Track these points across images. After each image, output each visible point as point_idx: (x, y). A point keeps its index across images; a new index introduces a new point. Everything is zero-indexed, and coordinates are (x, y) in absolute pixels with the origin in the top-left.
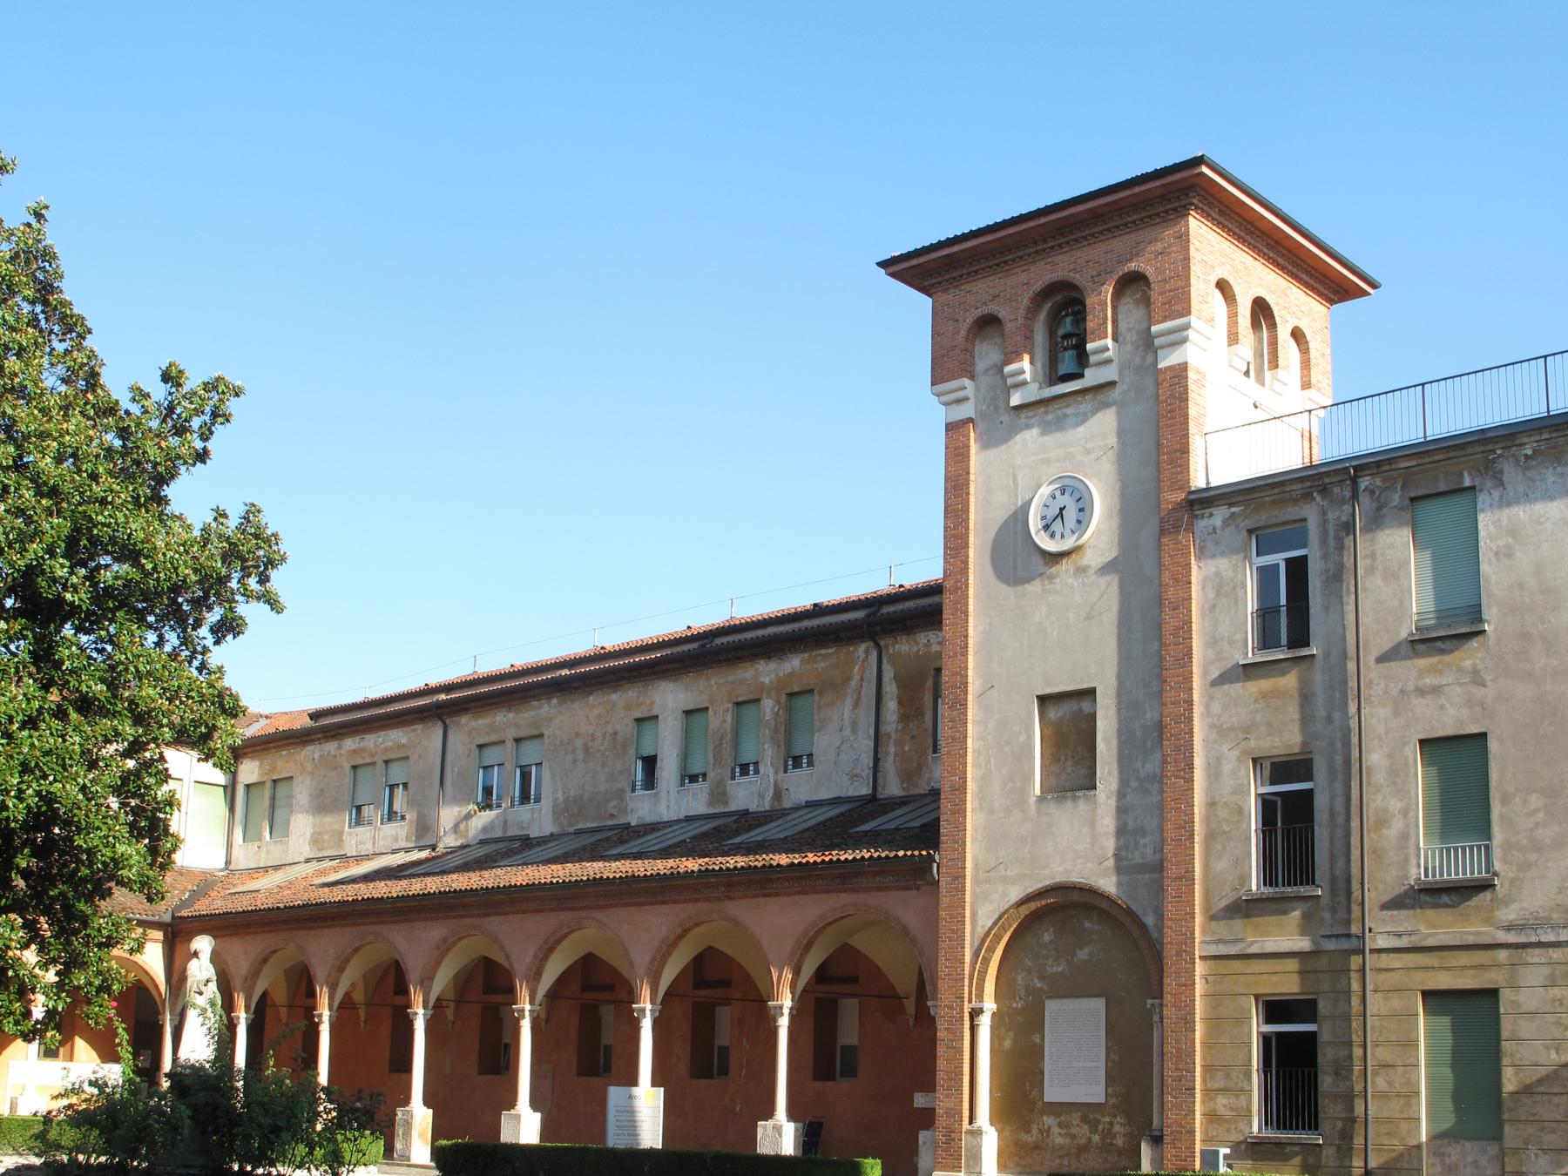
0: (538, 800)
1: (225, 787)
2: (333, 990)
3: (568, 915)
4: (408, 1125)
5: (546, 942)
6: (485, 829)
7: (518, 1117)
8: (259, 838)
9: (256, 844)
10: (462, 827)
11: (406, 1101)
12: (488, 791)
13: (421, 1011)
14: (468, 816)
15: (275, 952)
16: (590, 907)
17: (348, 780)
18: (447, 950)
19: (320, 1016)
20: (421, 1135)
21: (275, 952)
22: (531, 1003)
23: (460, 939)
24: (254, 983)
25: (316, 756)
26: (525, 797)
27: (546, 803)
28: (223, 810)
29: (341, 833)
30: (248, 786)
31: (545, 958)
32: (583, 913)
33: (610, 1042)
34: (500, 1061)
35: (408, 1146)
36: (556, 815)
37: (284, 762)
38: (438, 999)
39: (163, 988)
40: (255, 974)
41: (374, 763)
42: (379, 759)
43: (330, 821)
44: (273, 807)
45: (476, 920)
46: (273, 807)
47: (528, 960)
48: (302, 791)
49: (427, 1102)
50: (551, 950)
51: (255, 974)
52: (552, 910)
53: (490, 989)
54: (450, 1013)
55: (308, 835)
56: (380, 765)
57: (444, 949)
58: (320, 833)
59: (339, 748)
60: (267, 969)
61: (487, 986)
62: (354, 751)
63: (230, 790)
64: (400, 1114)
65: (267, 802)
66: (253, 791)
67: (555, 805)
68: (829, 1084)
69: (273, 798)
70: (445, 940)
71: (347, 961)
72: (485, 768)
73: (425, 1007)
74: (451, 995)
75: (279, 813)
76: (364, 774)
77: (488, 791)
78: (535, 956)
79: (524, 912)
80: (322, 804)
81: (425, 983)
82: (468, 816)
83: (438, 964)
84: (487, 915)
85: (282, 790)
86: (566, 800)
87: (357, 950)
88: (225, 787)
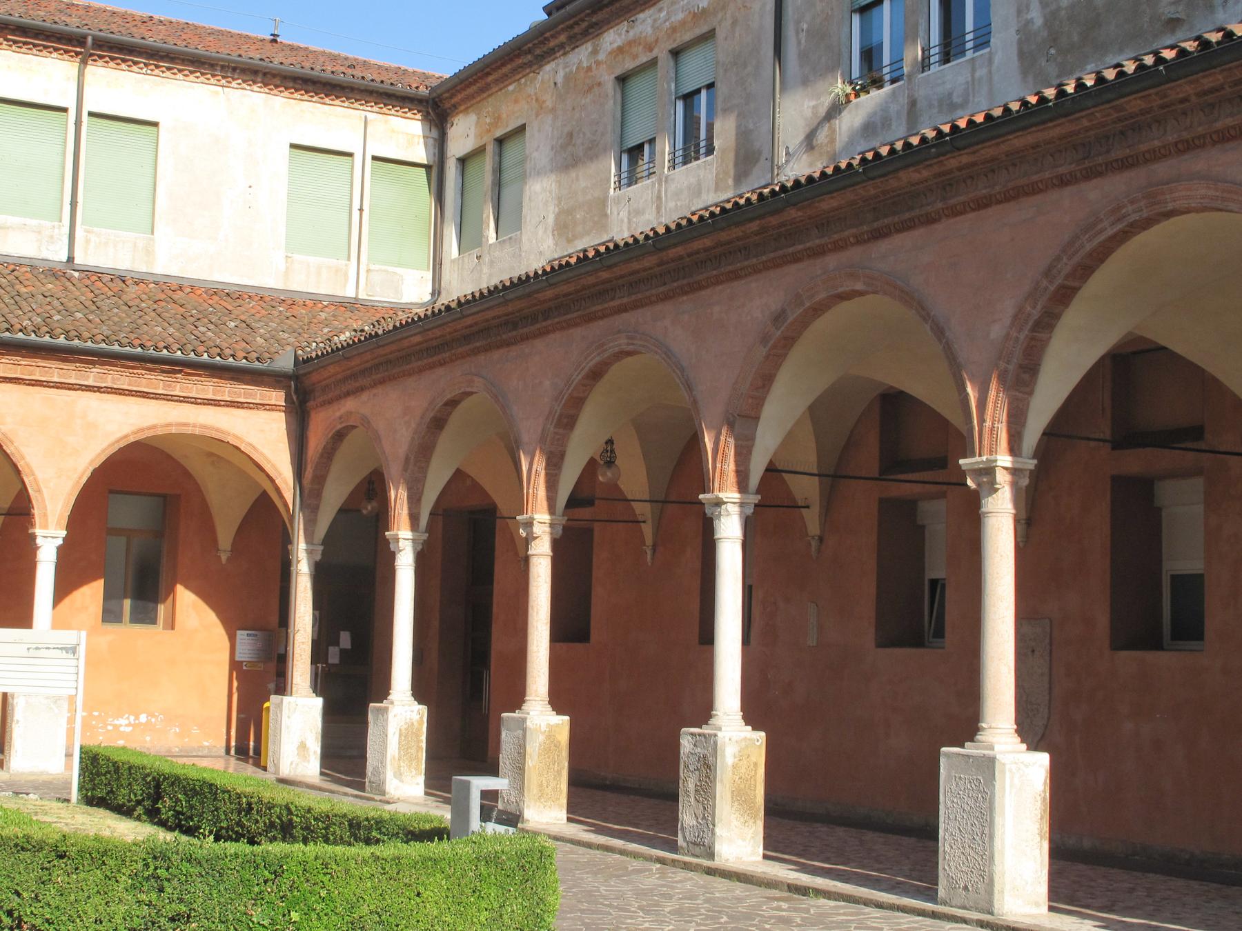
0: (983, 41)
1: (428, 168)
2: (554, 465)
3: (1115, 186)
4: (707, 767)
5: (1048, 273)
6: (869, 128)
7: (988, 765)
8: (479, 240)
9: (476, 252)
10: (822, 137)
11: (703, 711)
12: (870, 55)
13: (731, 495)
14: (835, 110)
15: (453, 403)
16: (1186, 147)
17: (612, 104)
18: (789, 341)
19: (529, 524)
20: (740, 796)
21: (453, 403)
22: (1014, 450)
23: (818, 310)
24: (424, 470)
25: (560, 79)
26: (950, 49)
27: (1004, 40)
28: (427, 202)
29: (603, 201)
30: (463, 161)
31: (1046, 323)
32: (1161, 169)
33: (1193, 565)
34: (926, 612)
35: (708, 819)
36: (1027, 58)
37: (509, 105)
38: (771, 469)
39: (289, 495)
40: (423, 452)
41: (653, 63)
42: (662, 52)
43: (583, 178)
44: (498, 184)
45: (854, 254)
46: (498, 184)
47: (997, 332)
48: (538, 146)
49: (753, 713)
50: (1064, 296)
51: (423, 452)
52: (1063, 182)
53: (894, 462)
54: (806, 489)
55: (551, 219)
56: (665, 62)
57: (780, 341)
58: (569, 212)
59: (595, 52)
60: (445, 442)
61: (878, 500)
62: (620, 50)
63: (435, 171)
64: (686, 744)
65: (488, 179)
66: (472, 168)
67: (1025, 33)
68: (1150, 656)
69: (498, 171)
70: (778, 318)
71: (577, 403)
72: (863, 10)
73: (742, 486)
74: (808, 458)
75: (507, 194)
76: (638, 87)
77: (870, 55)
78: (1018, 317)
79: (982, 204)
80: (572, 154)
81: (742, 422)
82: (835, 110)
83: (765, 381)
84: (879, 235)
85: (511, 152)
86: (1051, 19)
87: (596, 375)
88: (428, 168)
